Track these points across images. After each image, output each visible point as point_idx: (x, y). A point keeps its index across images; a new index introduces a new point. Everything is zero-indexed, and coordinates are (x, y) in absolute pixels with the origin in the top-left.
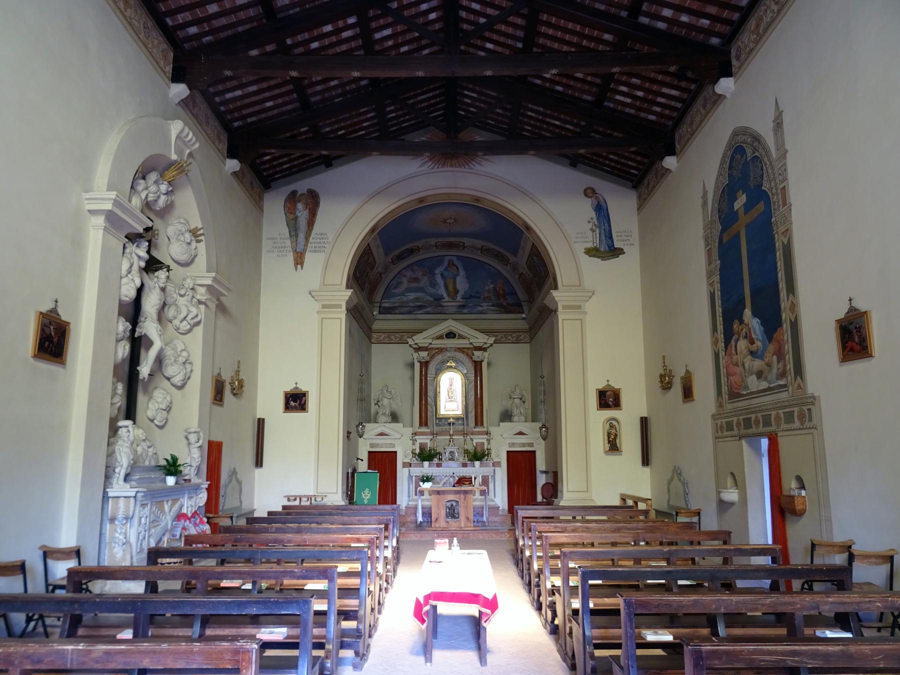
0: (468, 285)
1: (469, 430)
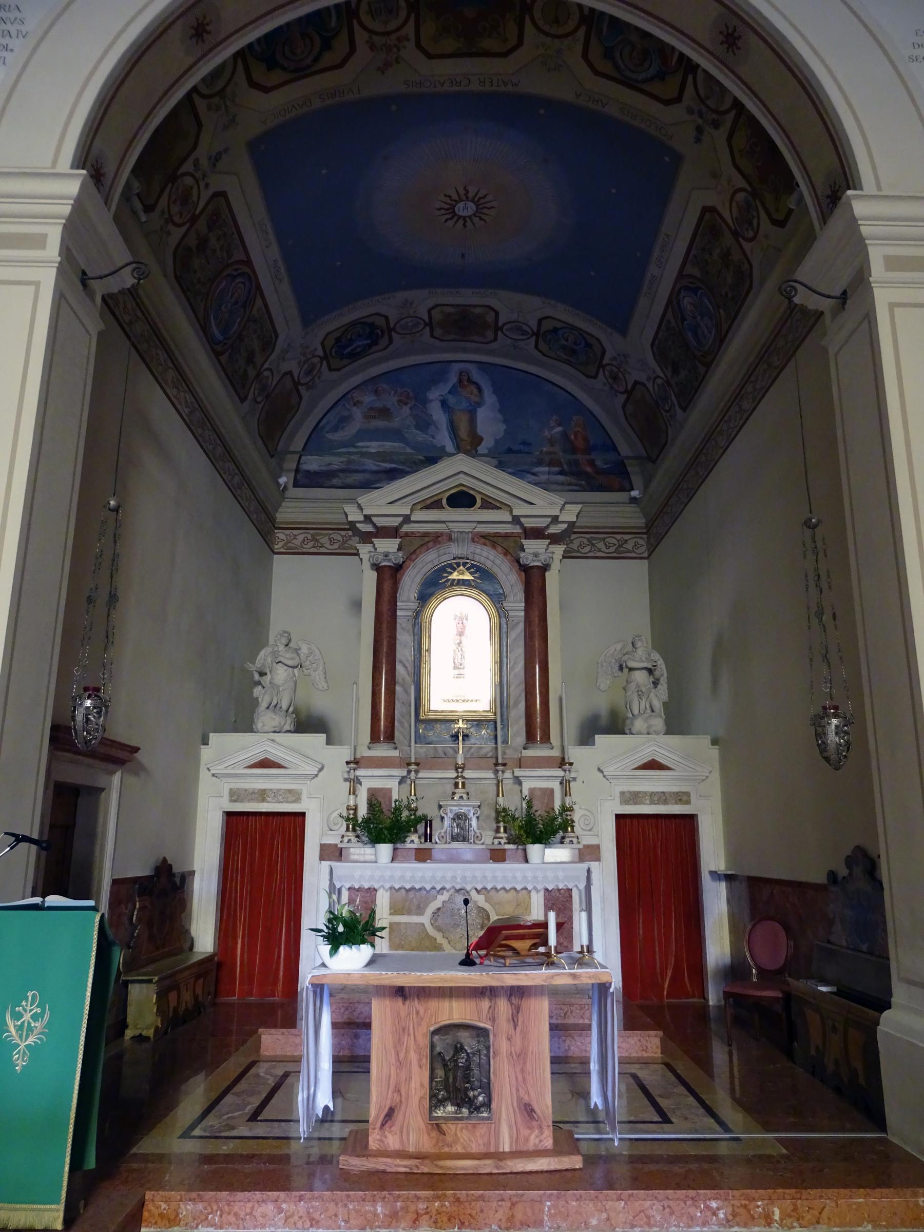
0: (503, 427)
1: (510, 753)
